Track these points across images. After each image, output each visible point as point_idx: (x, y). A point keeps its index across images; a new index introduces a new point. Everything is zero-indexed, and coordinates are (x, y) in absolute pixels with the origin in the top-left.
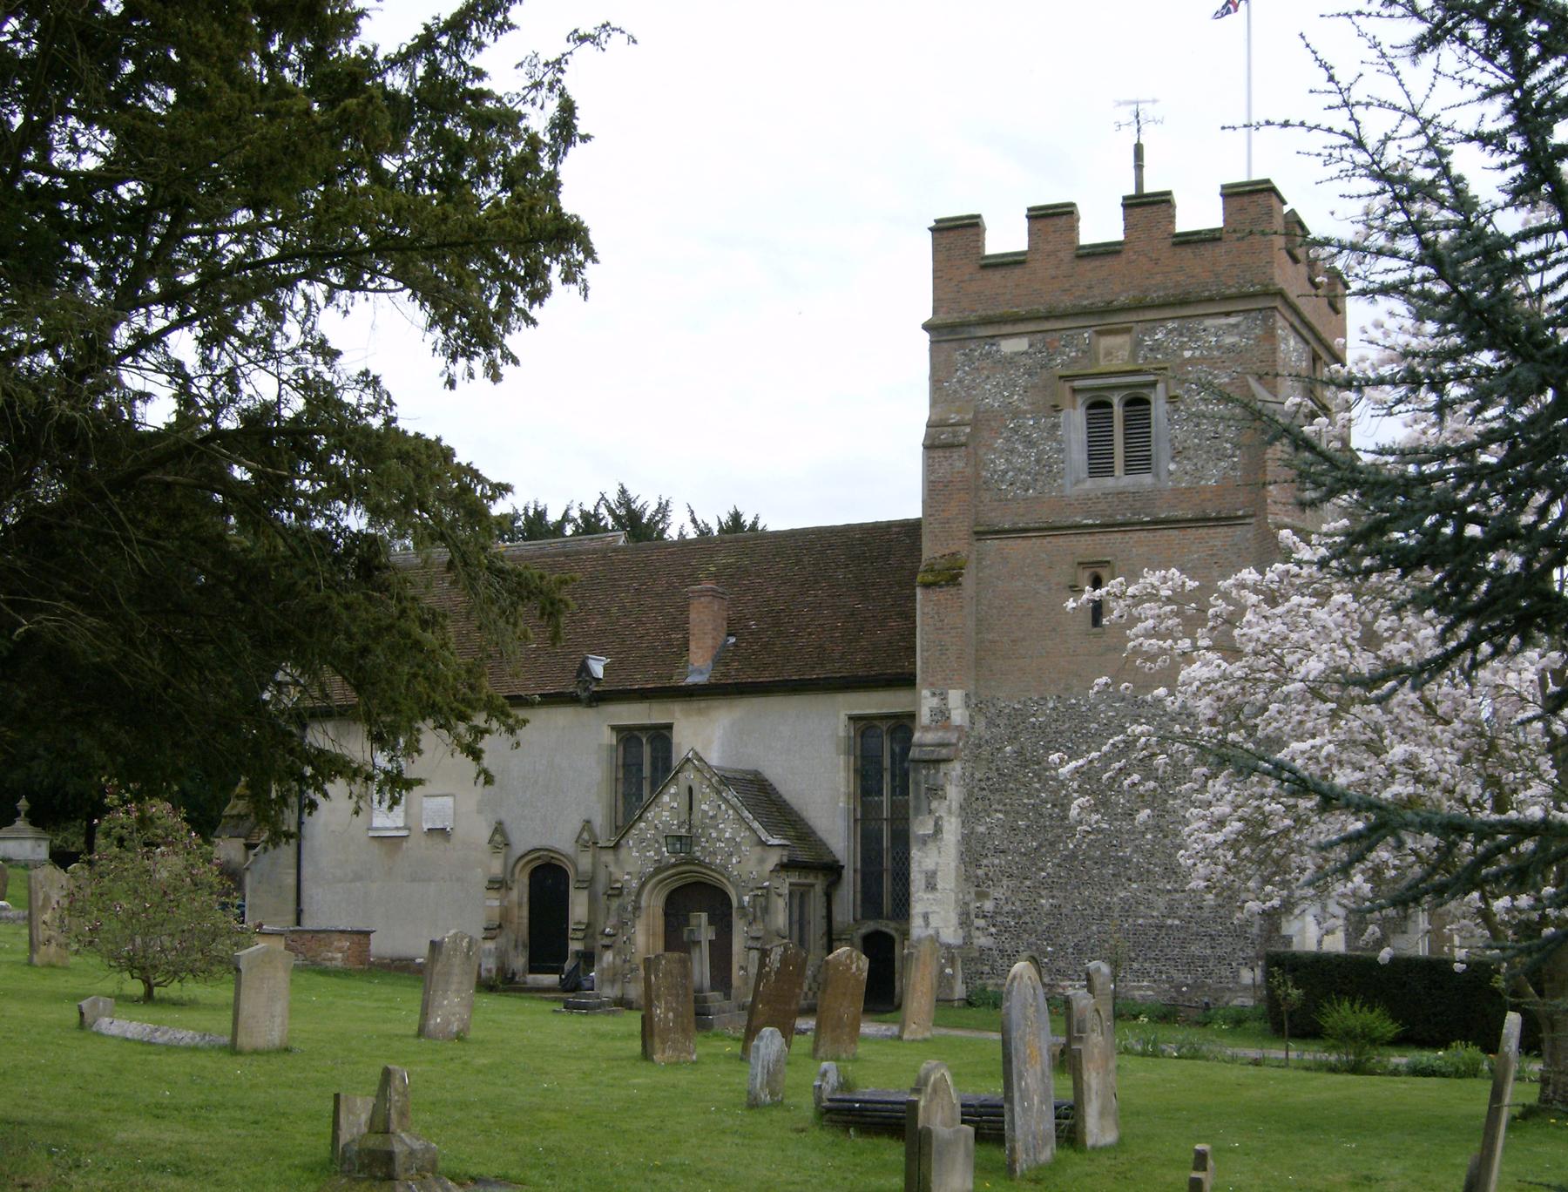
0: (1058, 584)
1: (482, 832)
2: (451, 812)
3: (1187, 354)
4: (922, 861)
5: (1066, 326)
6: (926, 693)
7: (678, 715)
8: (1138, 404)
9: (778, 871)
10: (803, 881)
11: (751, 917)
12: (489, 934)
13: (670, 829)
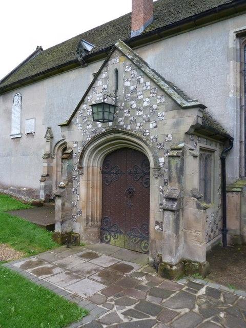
10: (208, 146)
11: (166, 177)
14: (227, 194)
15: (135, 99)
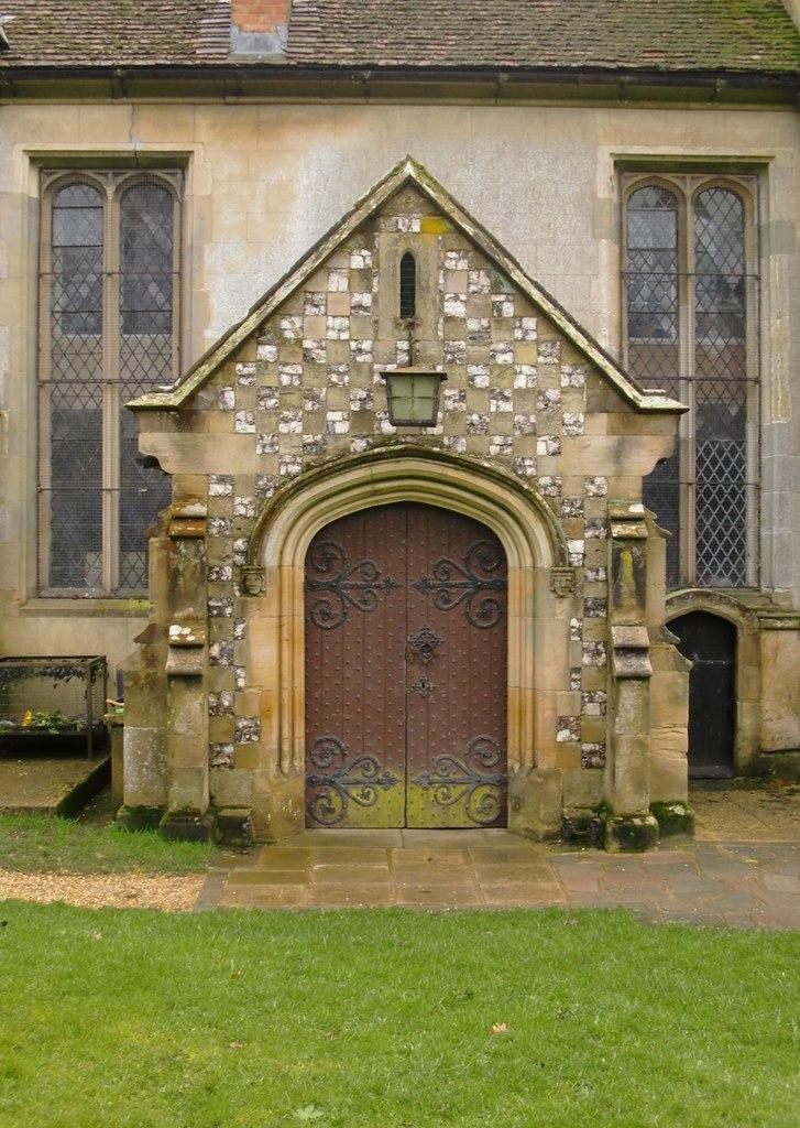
15: (488, 361)
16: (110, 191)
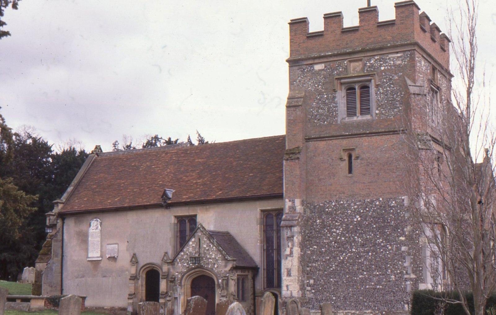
0: (335, 158)
1: (128, 257)
2: (117, 250)
3: (382, 68)
4: (286, 264)
5: (338, 59)
6: (287, 200)
7: (199, 211)
8: (365, 88)
9: (232, 270)
10: (242, 274)
11: (222, 288)
12: (130, 297)
13: (192, 255)
14: (256, 298)
15: (209, 254)
16: (187, 221)
